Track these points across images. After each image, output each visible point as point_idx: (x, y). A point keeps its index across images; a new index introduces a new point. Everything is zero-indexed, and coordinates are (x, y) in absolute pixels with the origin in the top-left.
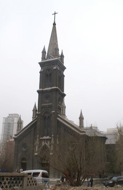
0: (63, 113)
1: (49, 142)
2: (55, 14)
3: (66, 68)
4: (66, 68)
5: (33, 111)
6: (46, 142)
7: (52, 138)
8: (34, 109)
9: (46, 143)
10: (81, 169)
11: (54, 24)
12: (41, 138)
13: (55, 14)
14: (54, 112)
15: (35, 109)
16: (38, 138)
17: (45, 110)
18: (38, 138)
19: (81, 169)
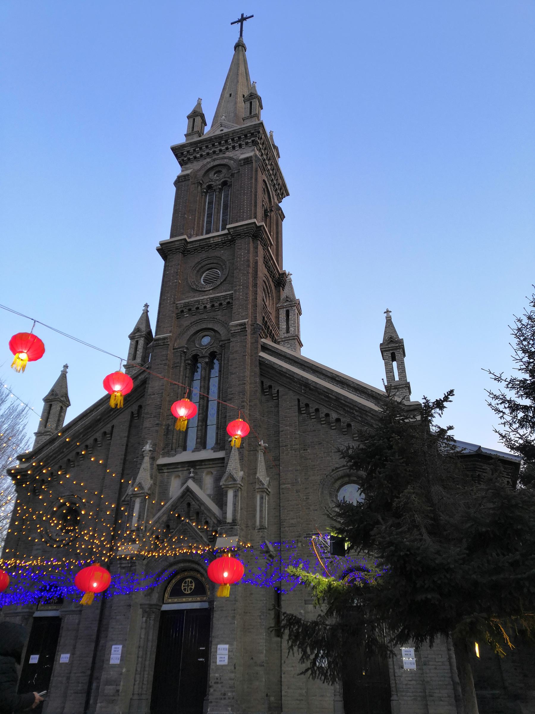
0: (288, 331)
1: (208, 480)
2: (242, 19)
3: (288, 194)
4: (288, 194)
5: (132, 337)
6: (194, 479)
7: (228, 454)
8: (137, 330)
9: (191, 484)
10: (181, 356)
11: (240, 46)
12: (162, 461)
13: (242, 19)
14: (281, 630)
15: (143, 328)
16: (147, 459)
17: (193, 324)
18: (147, 459)
19: (181, 356)
